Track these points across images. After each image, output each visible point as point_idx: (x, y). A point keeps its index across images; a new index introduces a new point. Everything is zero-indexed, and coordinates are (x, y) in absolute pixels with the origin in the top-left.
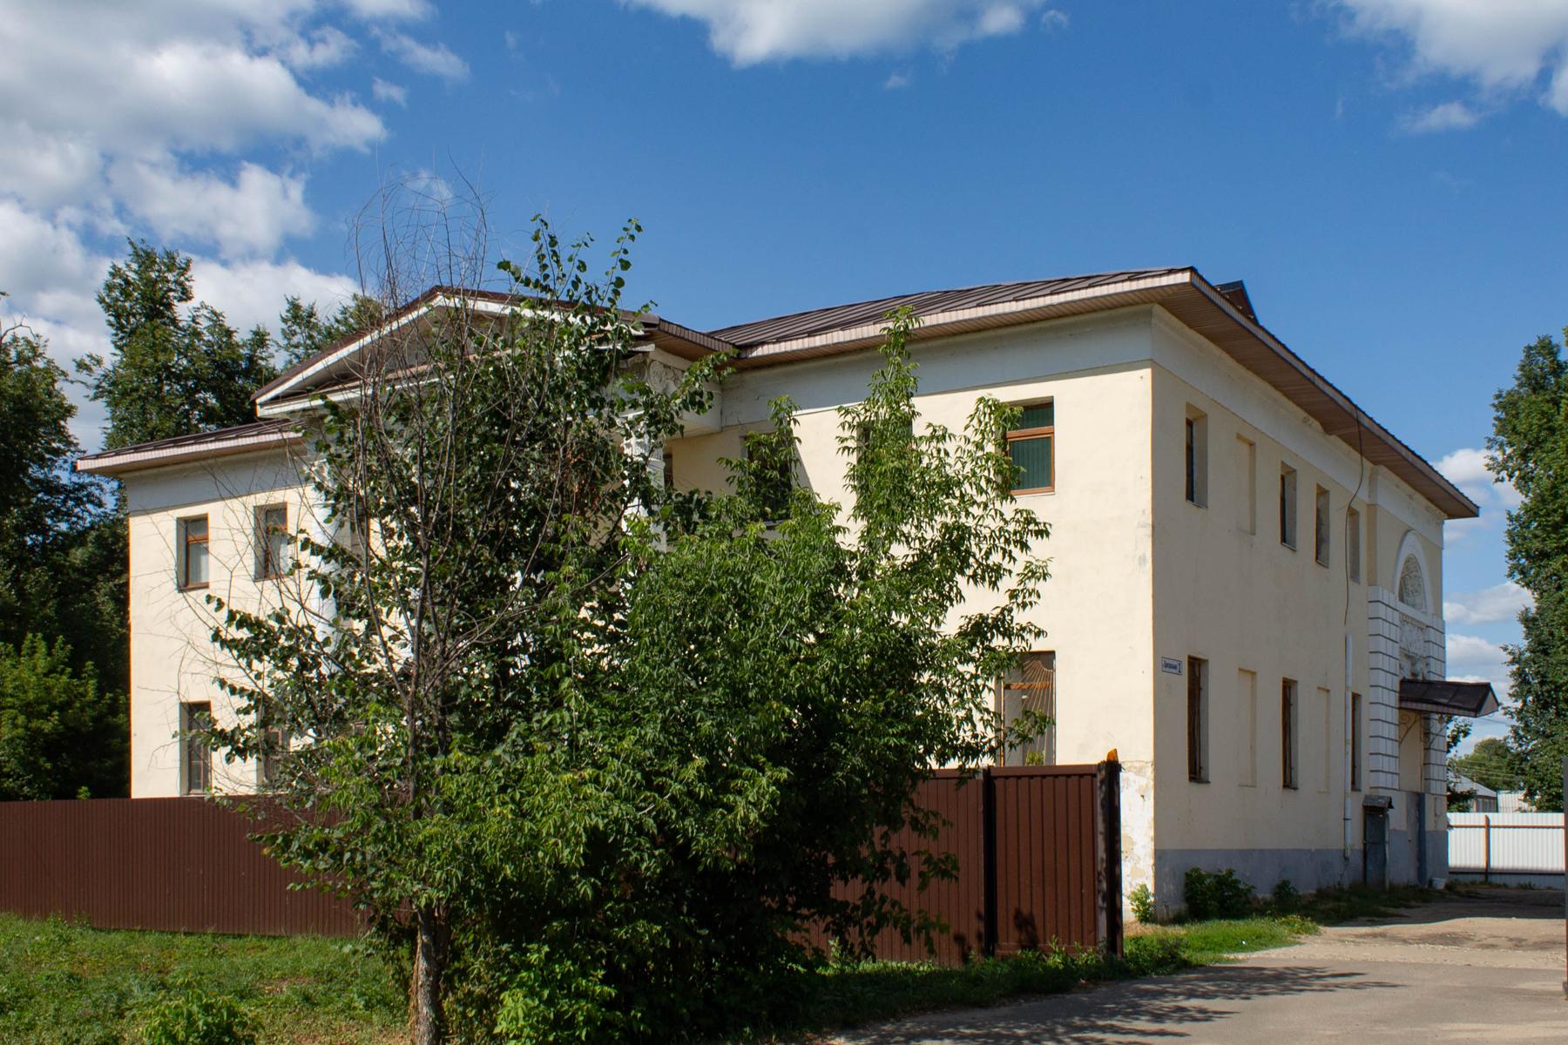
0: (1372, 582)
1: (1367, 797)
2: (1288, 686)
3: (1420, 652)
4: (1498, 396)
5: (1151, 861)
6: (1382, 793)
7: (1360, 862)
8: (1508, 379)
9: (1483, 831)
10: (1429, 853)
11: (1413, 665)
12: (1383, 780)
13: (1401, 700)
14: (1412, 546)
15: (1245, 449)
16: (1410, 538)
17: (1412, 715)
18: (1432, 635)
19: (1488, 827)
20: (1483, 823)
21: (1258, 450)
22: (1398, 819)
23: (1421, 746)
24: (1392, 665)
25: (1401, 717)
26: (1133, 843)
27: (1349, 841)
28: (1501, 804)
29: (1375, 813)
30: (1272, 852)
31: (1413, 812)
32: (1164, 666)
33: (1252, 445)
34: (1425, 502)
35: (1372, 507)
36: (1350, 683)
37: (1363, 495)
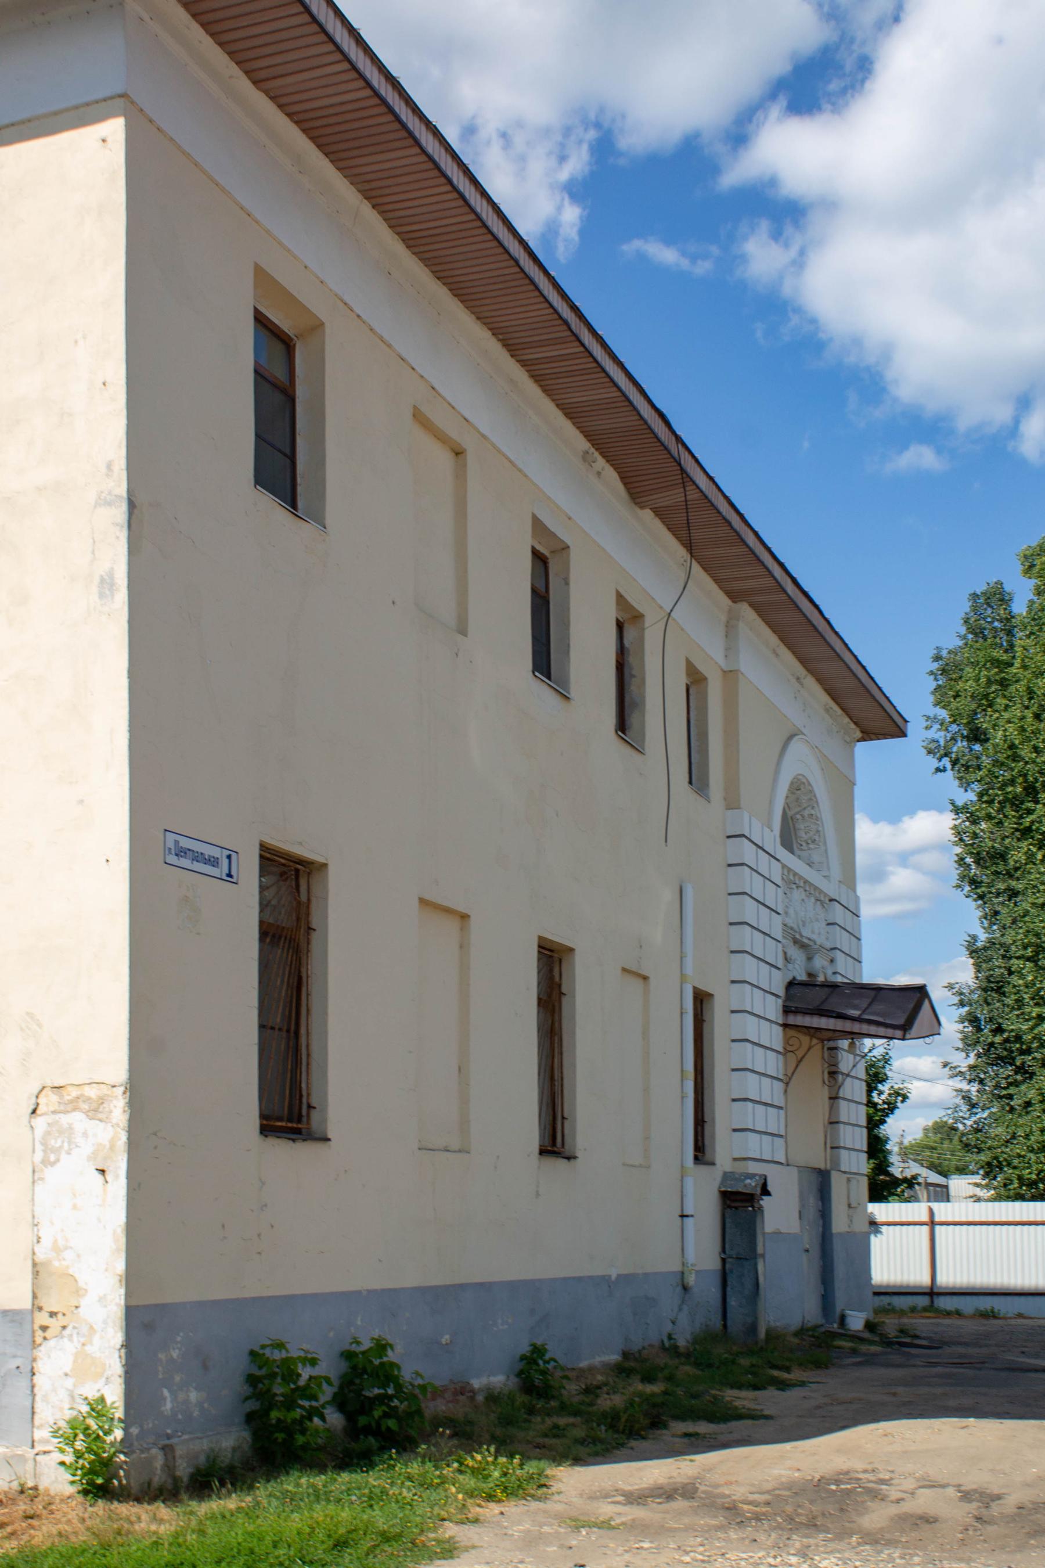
0: (732, 803)
1: (726, 1176)
2: (552, 959)
3: (820, 940)
4: (937, 658)
5: (116, 1337)
6: (753, 1168)
7: (713, 1292)
8: (951, 636)
9: (925, 1229)
10: (840, 1270)
11: (810, 959)
12: (754, 1146)
13: (787, 1011)
14: (800, 761)
15: (443, 458)
16: (797, 747)
17: (805, 1040)
18: (839, 914)
19: (932, 1223)
20: (925, 1217)
21: (471, 458)
22: (781, 1214)
23: (826, 1093)
24: (773, 952)
25: (787, 1041)
26: (79, 1292)
27: (691, 1255)
28: (952, 1192)
29: (740, 1203)
30: (514, 1287)
31: (813, 1201)
32: (165, 852)
33: (458, 453)
34: (825, 698)
35: (731, 676)
36: (689, 970)
37: (717, 654)
